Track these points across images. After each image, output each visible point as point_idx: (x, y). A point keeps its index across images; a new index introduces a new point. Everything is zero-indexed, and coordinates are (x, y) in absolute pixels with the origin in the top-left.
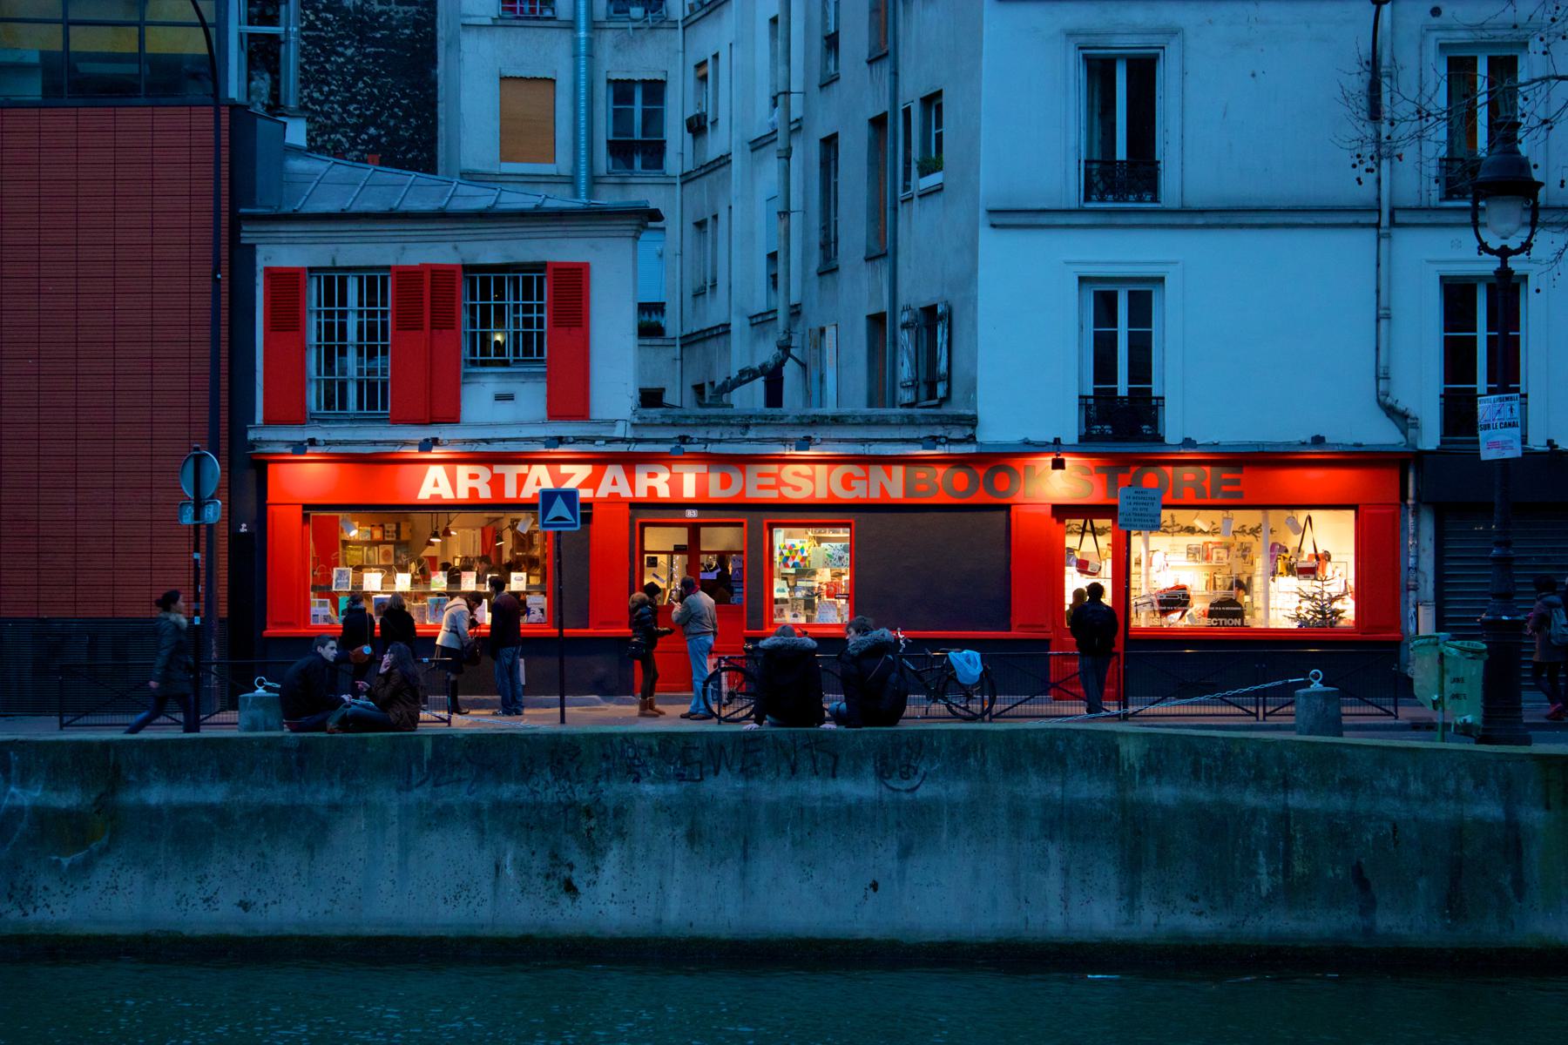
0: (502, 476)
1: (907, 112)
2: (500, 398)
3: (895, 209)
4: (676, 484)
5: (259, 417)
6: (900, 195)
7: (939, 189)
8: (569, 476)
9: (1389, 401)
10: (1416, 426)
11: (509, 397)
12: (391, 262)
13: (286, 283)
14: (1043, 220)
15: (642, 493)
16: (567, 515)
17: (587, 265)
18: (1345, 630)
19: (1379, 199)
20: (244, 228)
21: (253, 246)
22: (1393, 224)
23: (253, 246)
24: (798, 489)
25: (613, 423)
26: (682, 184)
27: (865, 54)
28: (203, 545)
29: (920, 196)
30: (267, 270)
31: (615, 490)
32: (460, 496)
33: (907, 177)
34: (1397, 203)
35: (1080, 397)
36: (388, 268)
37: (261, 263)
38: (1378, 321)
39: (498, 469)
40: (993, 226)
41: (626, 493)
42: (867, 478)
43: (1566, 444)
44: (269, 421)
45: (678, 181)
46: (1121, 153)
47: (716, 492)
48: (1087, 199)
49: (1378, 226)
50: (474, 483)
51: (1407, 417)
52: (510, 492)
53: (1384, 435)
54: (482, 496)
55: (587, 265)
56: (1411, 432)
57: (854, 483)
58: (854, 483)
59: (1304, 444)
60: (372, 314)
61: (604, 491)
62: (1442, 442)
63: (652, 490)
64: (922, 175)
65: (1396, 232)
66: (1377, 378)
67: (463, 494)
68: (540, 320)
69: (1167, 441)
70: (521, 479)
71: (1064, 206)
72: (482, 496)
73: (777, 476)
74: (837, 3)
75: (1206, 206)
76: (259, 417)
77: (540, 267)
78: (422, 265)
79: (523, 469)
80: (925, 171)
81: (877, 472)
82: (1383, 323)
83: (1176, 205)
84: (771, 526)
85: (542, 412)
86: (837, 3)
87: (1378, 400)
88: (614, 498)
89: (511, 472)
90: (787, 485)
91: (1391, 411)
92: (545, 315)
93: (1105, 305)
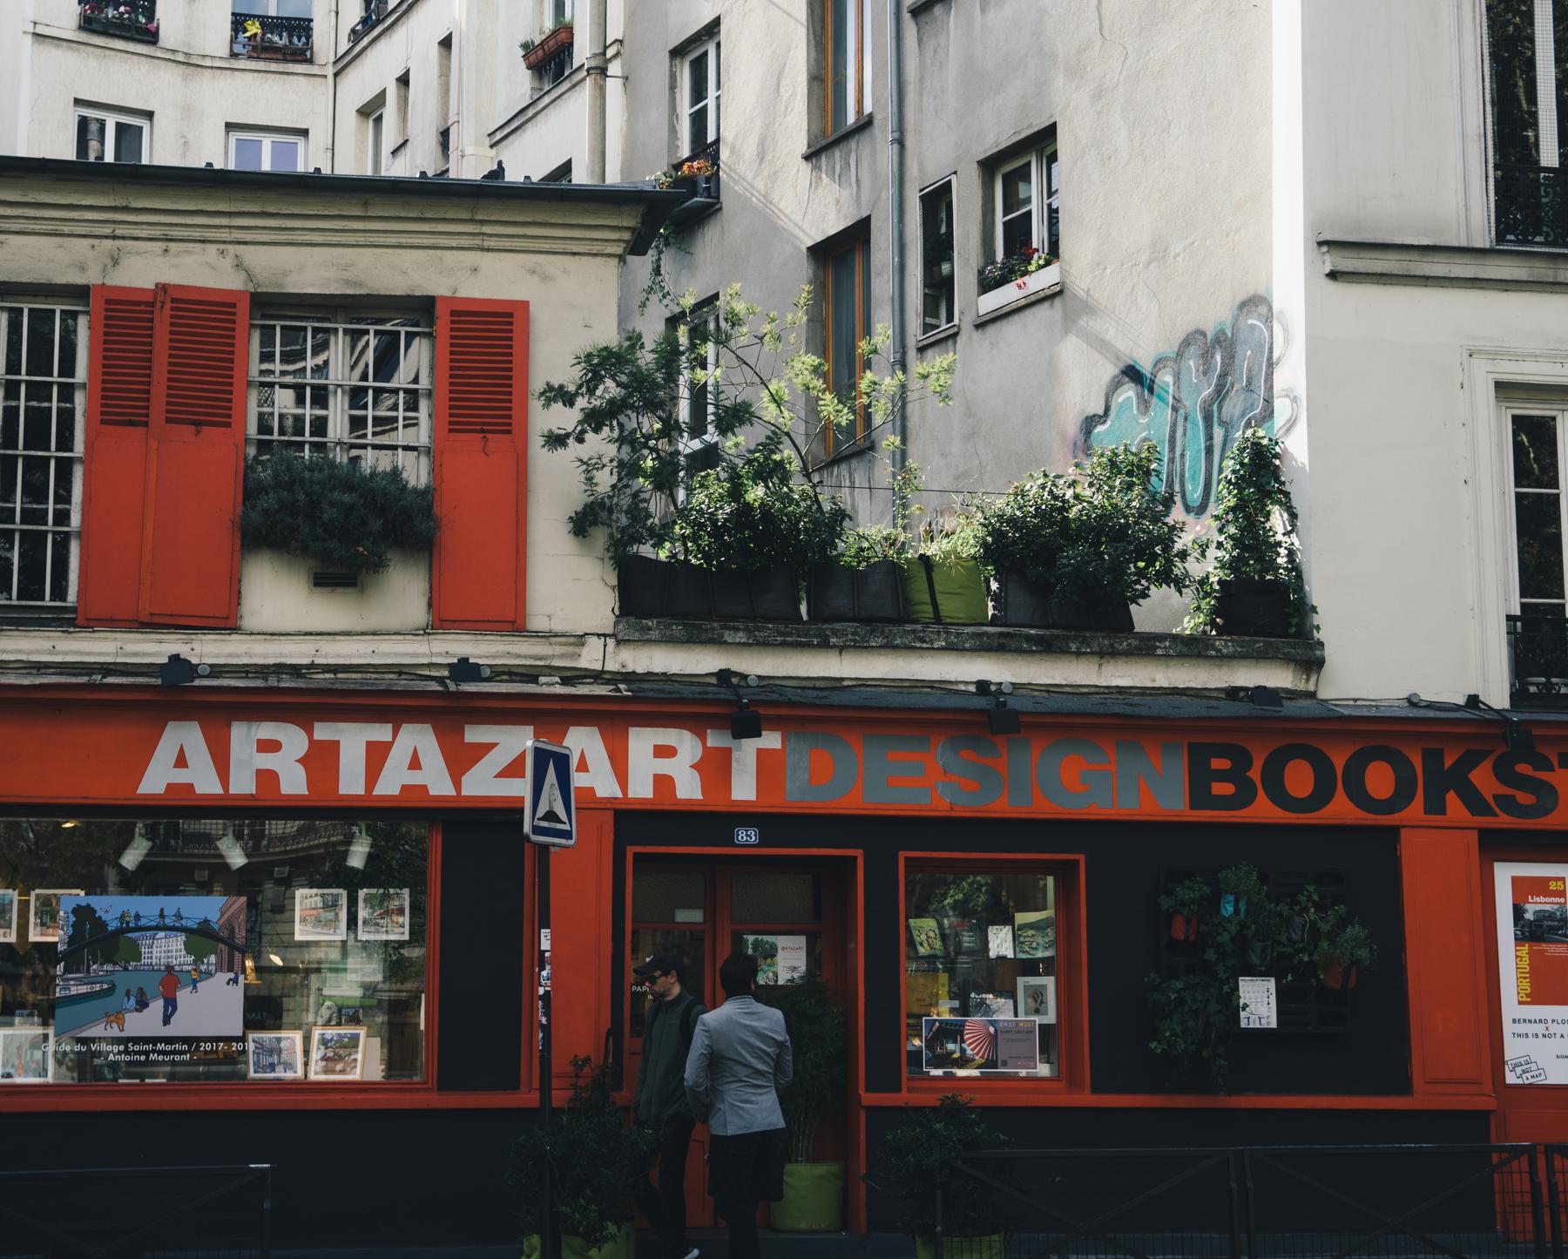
0: (334, 746)
1: (937, 201)
12: (92, 277)
15: (641, 789)
17: (524, 305)
18: (1052, 1070)
25: (580, 639)
27: (802, 146)
28: (340, 65)
29: (981, 326)
36: (80, 293)
39: (323, 731)
40: (1333, 275)
46: (1549, 155)
50: (267, 761)
52: (351, 783)
55: (524, 305)
60: (39, 391)
63: (663, 783)
70: (377, 755)
74: (4, 652)
77: (420, 309)
78: (163, 288)
79: (381, 732)
86: (4, 652)
89: (353, 740)
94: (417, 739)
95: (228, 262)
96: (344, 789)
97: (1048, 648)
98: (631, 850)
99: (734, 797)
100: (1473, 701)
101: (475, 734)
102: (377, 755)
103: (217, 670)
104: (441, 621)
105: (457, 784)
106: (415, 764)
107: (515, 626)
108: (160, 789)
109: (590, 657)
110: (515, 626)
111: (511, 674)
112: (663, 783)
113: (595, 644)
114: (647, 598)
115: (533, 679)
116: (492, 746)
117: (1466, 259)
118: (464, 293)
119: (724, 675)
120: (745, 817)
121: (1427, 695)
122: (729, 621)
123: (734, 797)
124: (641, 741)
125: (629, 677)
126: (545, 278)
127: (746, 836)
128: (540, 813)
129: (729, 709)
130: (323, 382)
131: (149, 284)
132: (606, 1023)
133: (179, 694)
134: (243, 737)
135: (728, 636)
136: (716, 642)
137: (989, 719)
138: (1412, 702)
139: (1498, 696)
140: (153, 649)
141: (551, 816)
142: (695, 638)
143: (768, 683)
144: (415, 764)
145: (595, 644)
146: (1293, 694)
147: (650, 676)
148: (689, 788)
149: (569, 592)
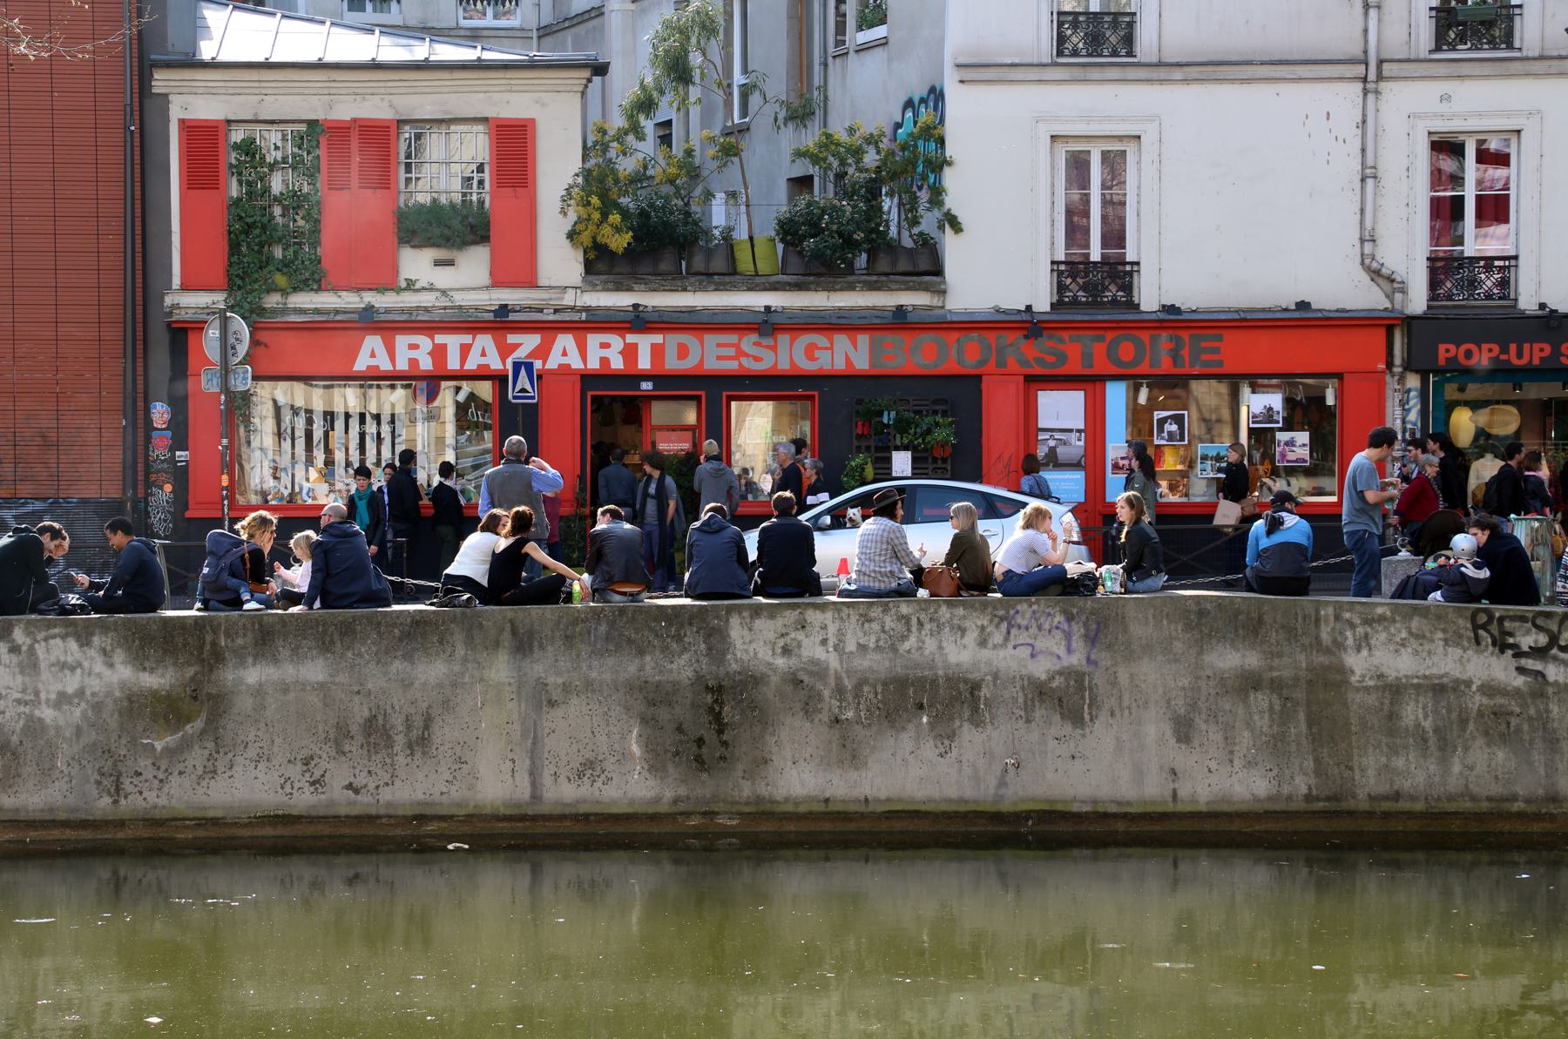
0: (635, 346)
2: (438, 263)
3: (826, 65)
4: (630, 352)
5: (176, 281)
6: (831, 49)
7: (883, 43)
8: (517, 346)
9: (1375, 265)
10: (1403, 291)
11: (450, 263)
13: (202, 137)
14: (1248, 71)
15: (594, 364)
16: (529, 388)
17: (533, 121)
19: (1366, 52)
20: (156, 76)
21: (166, 95)
22: (1380, 77)
23: (166, 95)
24: (758, 359)
26: (539, 37)
30: (182, 122)
31: (564, 361)
32: (589, 366)
33: (841, 28)
34: (1385, 56)
35: (1053, 263)
37: (176, 113)
38: (1363, 180)
39: (440, 339)
41: (577, 364)
42: (831, 348)
43: (1563, 308)
44: (185, 287)
45: (535, 35)
47: (673, 364)
48: (1060, 53)
49: (1365, 80)
51: (1393, 281)
52: (453, 364)
53: (1370, 298)
54: (613, 366)
56: (1398, 296)
57: (817, 353)
58: (817, 353)
59: (1286, 310)
61: (553, 362)
62: (1429, 307)
63: (605, 361)
64: (859, 28)
65: (1383, 85)
66: (1362, 241)
67: (402, 365)
68: (481, 182)
69: (1143, 308)
70: (465, 350)
71: (1036, 61)
72: (613, 366)
73: (737, 346)
75: (1184, 60)
76: (176, 281)
78: (355, 120)
79: (466, 339)
80: (865, 23)
81: (841, 340)
82: (1370, 182)
83: (1155, 60)
84: (730, 399)
85: (485, 279)
87: (1362, 263)
88: (565, 370)
90: (747, 355)
91: (1376, 274)
92: (487, 175)
93: (1078, 167)
94: (485, 341)
95: (386, 104)
96: (450, 367)
97: (799, 287)
98: (590, 394)
99: (1081, 394)
100: (1029, 308)
101: (512, 338)
102: (465, 350)
103: (388, 311)
104: (497, 282)
105: (585, 363)
106: (483, 354)
107: (532, 284)
108: (474, 367)
109: (569, 299)
110: (532, 284)
111: (530, 309)
112: (605, 361)
113: (571, 292)
114: (601, 263)
115: (541, 311)
116: (519, 345)
117: (1036, 69)
118: (502, 115)
119: (636, 306)
120: (646, 377)
121: (1005, 306)
122: (638, 281)
123: (1081, 394)
124: (593, 340)
125: (587, 309)
126: (544, 105)
127: (646, 386)
128: (518, 388)
129: (638, 321)
130: (618, 420)
131: (348, 118)
132: (578, 471)
133: (370, 322)
134: (402, 341)
135: (636, 287)
136: (630, 289)
137: (767, 325)
138: (998, 311)
139: (1042, 304)
140: (349, 300)
141: (523, 390)
142: (619, 287)
143: (656, 310)
144: (483, 354)
145: (571, 292)
146: (931, 308)
147: (598, 308)
148: (617, 364)
149: (560, 264)
